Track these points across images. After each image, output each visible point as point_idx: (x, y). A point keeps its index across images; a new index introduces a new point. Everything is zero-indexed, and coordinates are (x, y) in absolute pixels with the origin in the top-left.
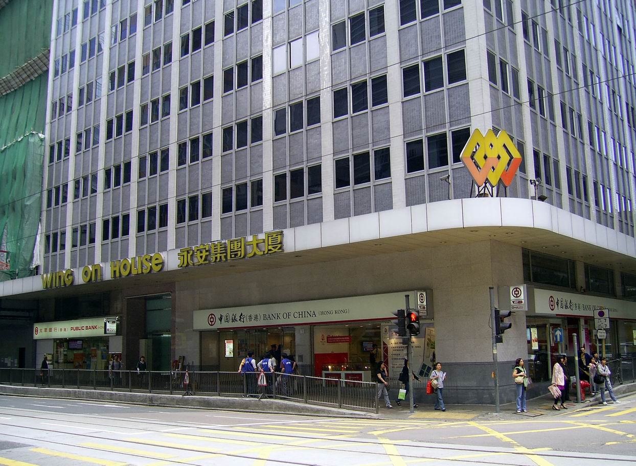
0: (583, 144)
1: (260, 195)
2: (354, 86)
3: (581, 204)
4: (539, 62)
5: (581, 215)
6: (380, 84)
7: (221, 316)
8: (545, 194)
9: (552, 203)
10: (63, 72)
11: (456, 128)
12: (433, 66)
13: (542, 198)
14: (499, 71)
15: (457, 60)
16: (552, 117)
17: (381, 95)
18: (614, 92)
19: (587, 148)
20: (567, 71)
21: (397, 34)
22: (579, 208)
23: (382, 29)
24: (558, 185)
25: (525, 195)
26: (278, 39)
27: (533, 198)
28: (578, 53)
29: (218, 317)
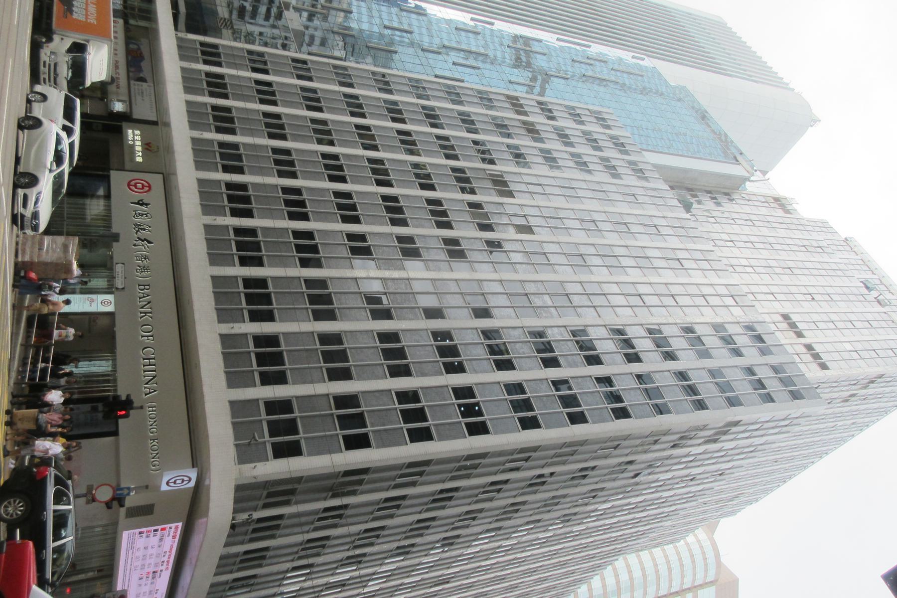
0: (293, 560)
1: (85, 251)
2: (403, 348)
3: (234, 564)
4: (307, 523)
5: (218, 567)
6: (459, 369)
7: (147, 204)
8: (237, 530)
9: (229, 536)
10: (481, 98)
11: (371, 436)
12: (420, 415)
13: (233, 527)
14: (354, 479)
15: (423, 435)
16: (316, 529)
17: (452, 369)
18: (344, 585)
19: (289, 565)
20: (359, 539)
21: (544, 377)
22: (225, 563)
23: (393, 375)
24: (252, 540)
25: (235, 511)
26: (390, 283)
27: (234, 519)
28: (375, 549)
29: (145, 197)
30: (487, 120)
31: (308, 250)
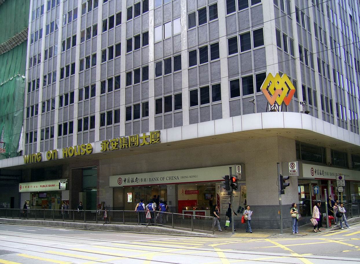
0: (330, 82)
1: (147, 110)
2: (200, 49)
3: (329, 115)
4: (305, 35)
5: (329, 122)
6: (215, 47)
8: (309, 110)
9: (312, 115)
11: (258, 72)
12: (245, 37)
13: (307, 112)
14: (282, 40)
15: (259, 34)
16: (313, 66)
17: (216, 54)
18: (347, 52)
19: (332, 84)
20: (321, 40)
21: (224, 19)
22: (328, 118)
23: (216, 16)
24: (316, 105)
25: (297, 111)
27: (302, 112)
28: (327, 30)
29: (123, 179)
30: (35, 22)
31: (139, 75)
